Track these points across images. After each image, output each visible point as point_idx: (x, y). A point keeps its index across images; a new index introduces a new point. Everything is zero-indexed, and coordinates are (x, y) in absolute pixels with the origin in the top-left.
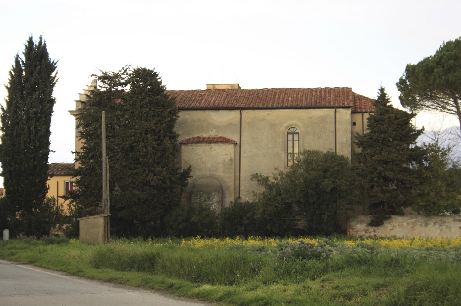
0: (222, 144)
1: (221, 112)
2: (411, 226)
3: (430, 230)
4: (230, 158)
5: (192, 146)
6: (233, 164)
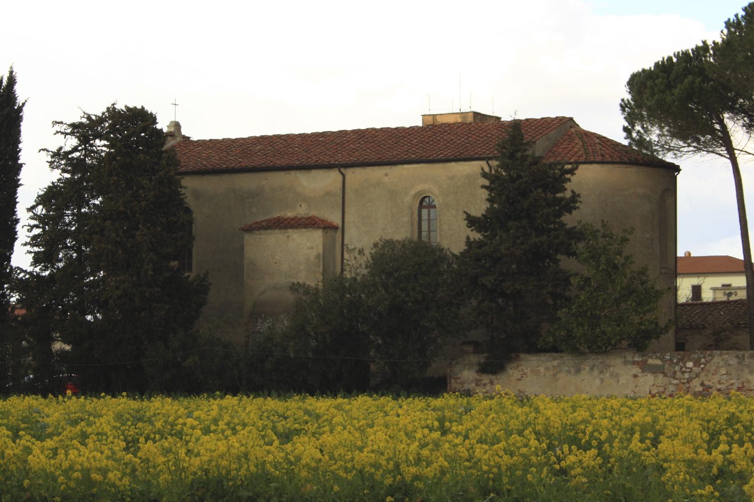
0: (304, 230)
1: (314, 173)
2: (552, 373)
3: (583, 380)
4: (315, 254)
5: (260, 234)
6: (321, 264)
